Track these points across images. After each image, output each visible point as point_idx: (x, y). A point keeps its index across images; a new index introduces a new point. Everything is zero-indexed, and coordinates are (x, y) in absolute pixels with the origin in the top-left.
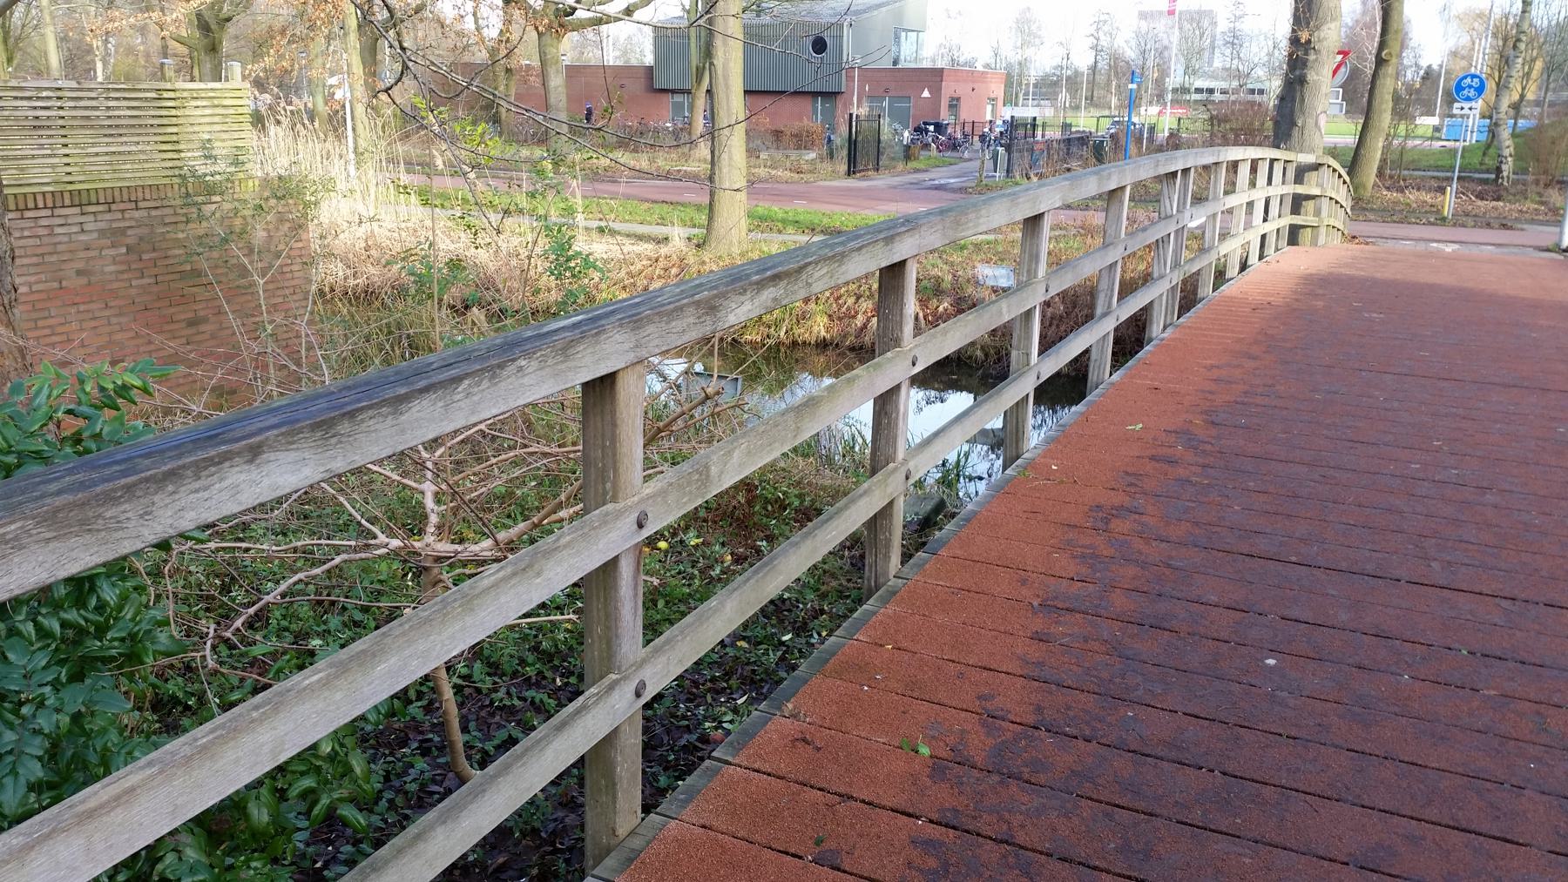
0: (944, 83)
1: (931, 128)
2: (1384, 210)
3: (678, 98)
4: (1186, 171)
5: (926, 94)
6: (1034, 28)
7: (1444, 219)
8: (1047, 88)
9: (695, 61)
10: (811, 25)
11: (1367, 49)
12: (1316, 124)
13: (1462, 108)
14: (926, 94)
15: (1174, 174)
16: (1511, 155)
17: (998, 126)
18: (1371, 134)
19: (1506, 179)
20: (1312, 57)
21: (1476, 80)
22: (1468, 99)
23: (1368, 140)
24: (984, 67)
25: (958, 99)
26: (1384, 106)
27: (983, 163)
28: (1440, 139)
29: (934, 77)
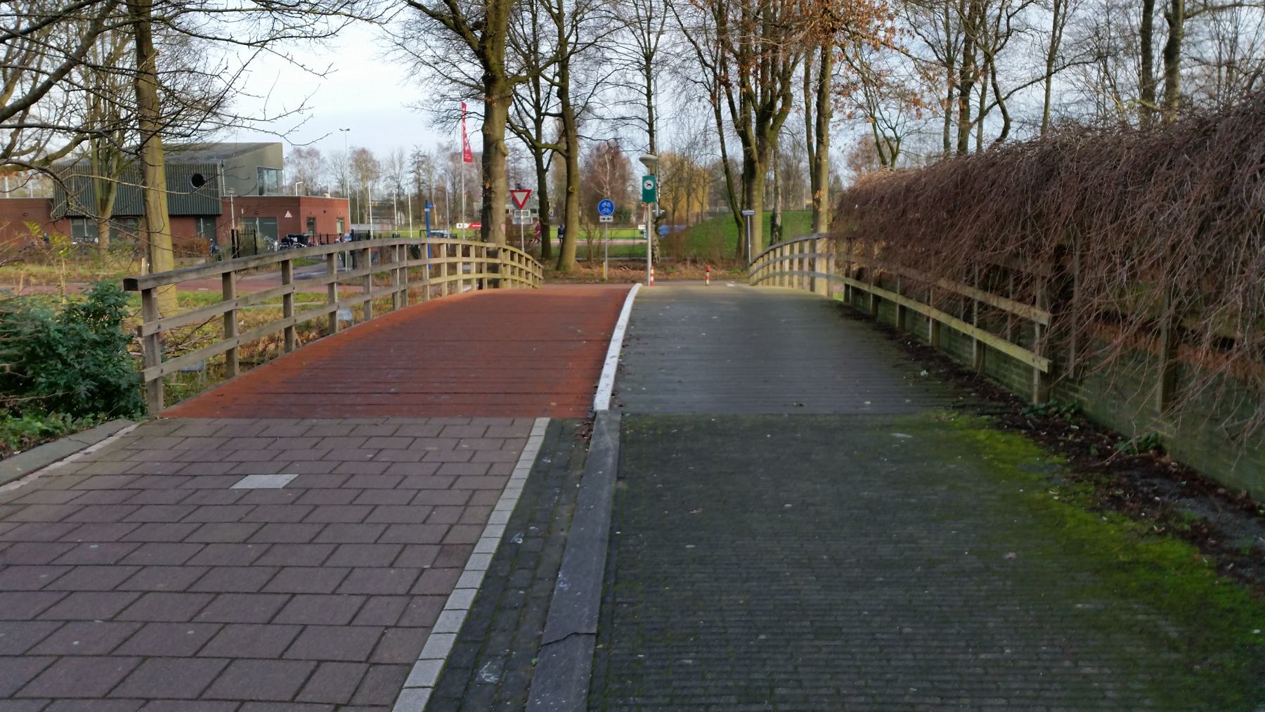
1: (295, 239)
3: (78, 223)
4: (401, 246)
5: (288, 215)
6: (369, 165)
8: (384, 210)
9: (99, 195)
10: (191, 167)
14: (288, 215)
15: (395, 246)
20: (493, 196)
22: (606, 214)
25: (314, 219)
29: (293, 203)
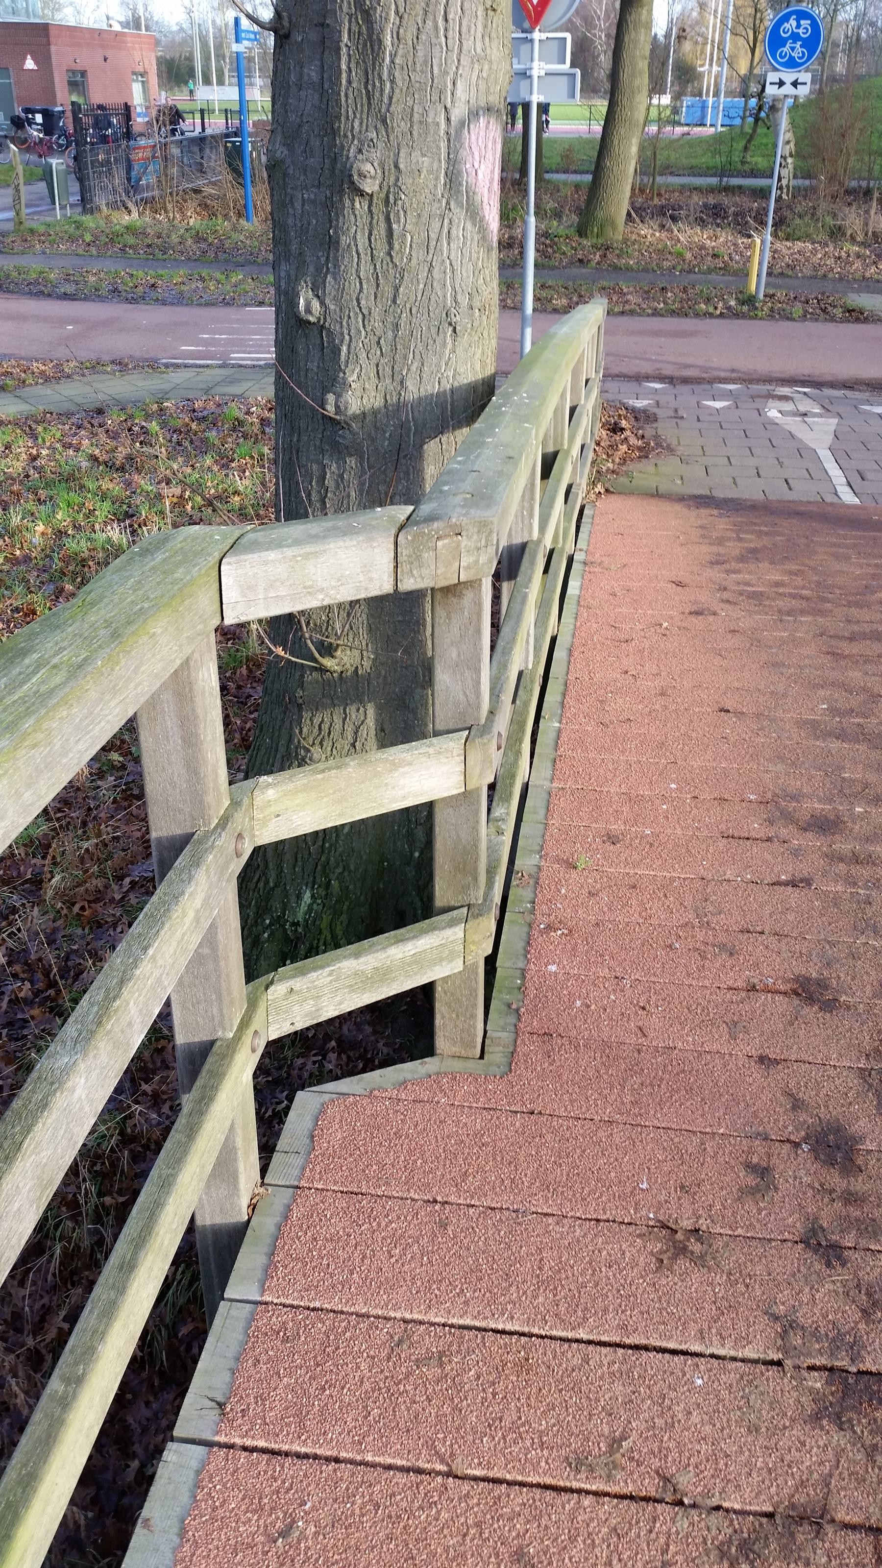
0: (53, 48)
2: (645, 270)
7: (750, 301)
11: (595, 12)
12: (453, 178)
13: (781, 84)
16: (791, 155)
17: (139, 115)
18: (621, 130)
19: (785, 190)
21: (805, 23)
23: (616, 142)
24: (123, 27)
25: (83, 73)
26: (637, 82)
27: (18, 190)
28: (679, 124)
